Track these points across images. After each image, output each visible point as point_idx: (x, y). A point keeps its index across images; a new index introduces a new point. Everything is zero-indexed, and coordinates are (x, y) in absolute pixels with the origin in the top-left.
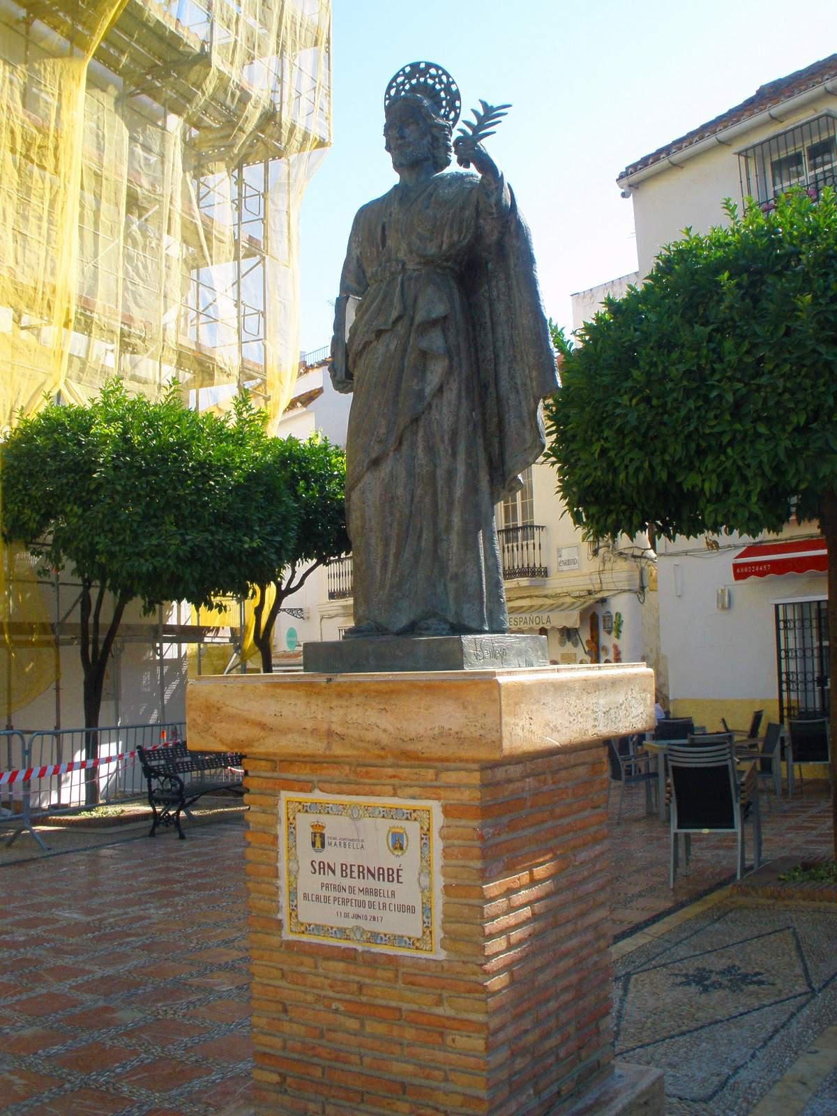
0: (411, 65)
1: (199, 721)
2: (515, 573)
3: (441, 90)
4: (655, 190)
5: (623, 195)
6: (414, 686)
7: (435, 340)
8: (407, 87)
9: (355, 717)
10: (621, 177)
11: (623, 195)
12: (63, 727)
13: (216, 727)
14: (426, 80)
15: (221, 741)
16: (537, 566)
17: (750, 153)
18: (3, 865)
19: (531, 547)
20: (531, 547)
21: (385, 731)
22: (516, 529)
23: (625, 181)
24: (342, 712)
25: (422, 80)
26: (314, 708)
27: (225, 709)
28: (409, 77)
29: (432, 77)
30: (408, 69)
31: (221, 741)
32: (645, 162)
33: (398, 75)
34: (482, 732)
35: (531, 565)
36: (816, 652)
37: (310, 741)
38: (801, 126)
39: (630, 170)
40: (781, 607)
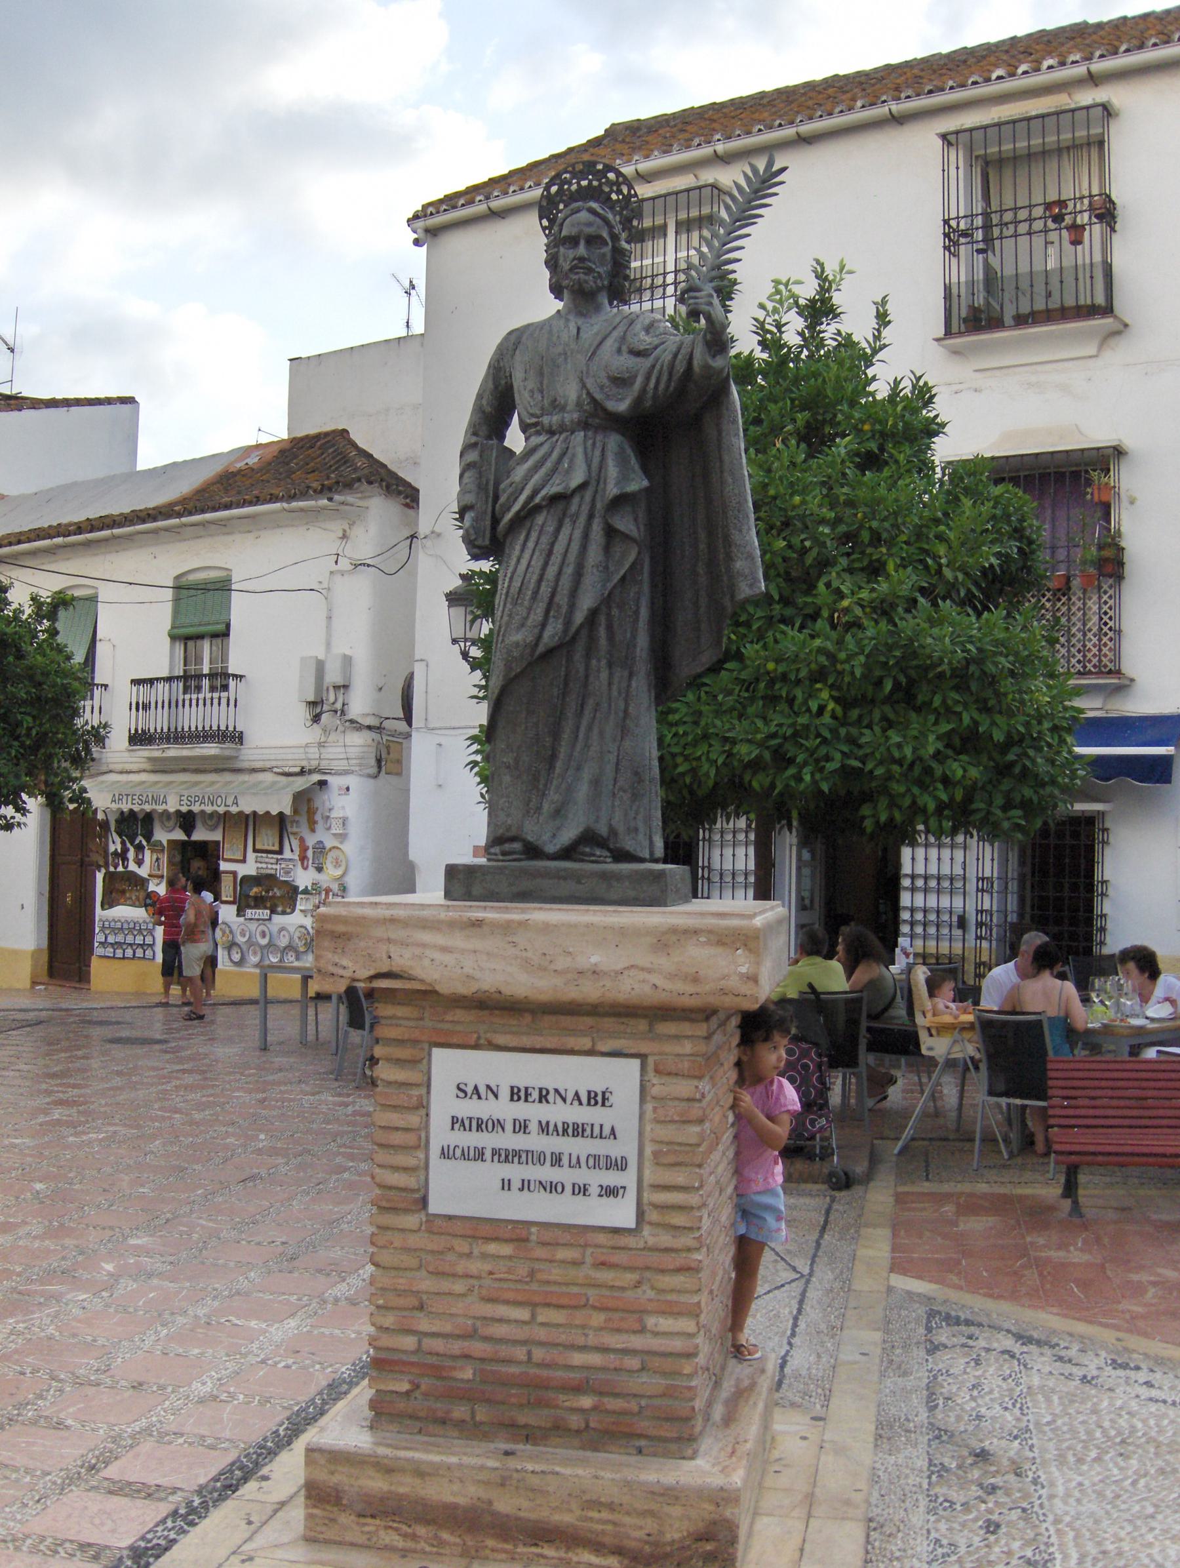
2: (183, 737)
4: (459, 243)
5: (417, 242)
7: (625, 523)
10: (416, 217)
11: (417, 242)
12: (254, 992)
16: (231, 729)
18: (1177, 1156)
19: (224, 701)
20: (224, 701)
22: (199, 676)
23: (420, 224)
32: (451, 201)
35: (223, 728)
39: (431, 209)
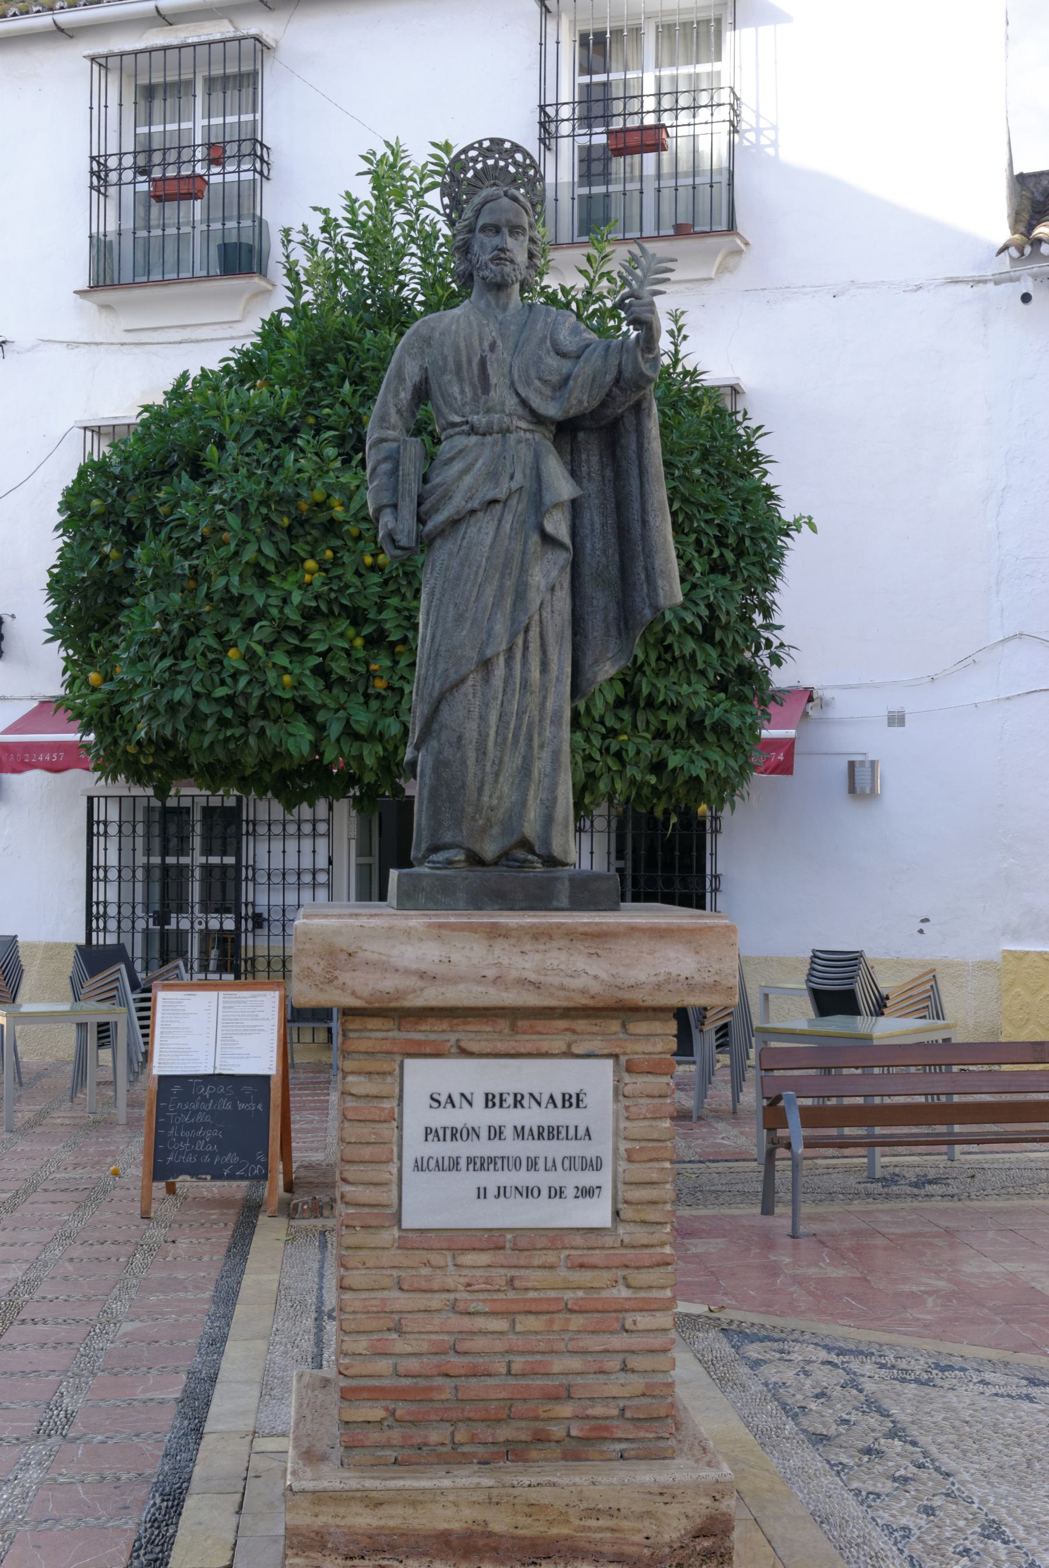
0: (492, 140)
1: (317, 969)
3: (485, 163)
6: (632, 931)
8: (479, 166)
9: (555, 963)
13: (345, 977)
14: (507, 166)
15: (353, 993)
17: (113, 62)
21: (596, 977)
24: (538, 957)
25: (502, 163)
26: (497, 951)
27: (361, 954)
28: (486, 153)
29: (516, 163)
30: (486, 144)
31: (353, 993)
33: (471, 147)
34: (717, 978)
36: (140, 874)
37: (492, 990)
38: (210, 43)
40: (96, 800)
